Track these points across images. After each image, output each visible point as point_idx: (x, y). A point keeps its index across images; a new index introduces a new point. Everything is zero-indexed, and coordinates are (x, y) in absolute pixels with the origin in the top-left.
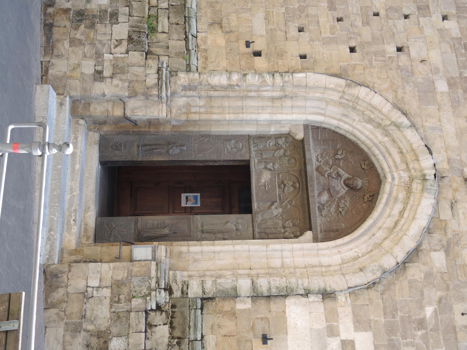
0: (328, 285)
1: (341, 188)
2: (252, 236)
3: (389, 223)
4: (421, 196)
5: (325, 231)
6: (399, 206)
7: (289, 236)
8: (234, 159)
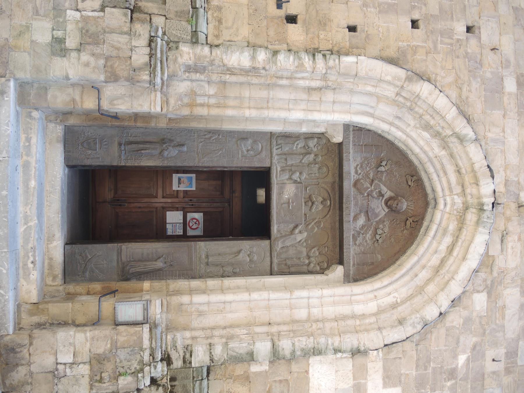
0: (362, 343)
1: (380, 211)
2: (268, 268)
3: (435, 261)
4: (476, 230)
5: (358, 264)
6: (448, 240)
7: (314, 269)
8: (250, 166)
